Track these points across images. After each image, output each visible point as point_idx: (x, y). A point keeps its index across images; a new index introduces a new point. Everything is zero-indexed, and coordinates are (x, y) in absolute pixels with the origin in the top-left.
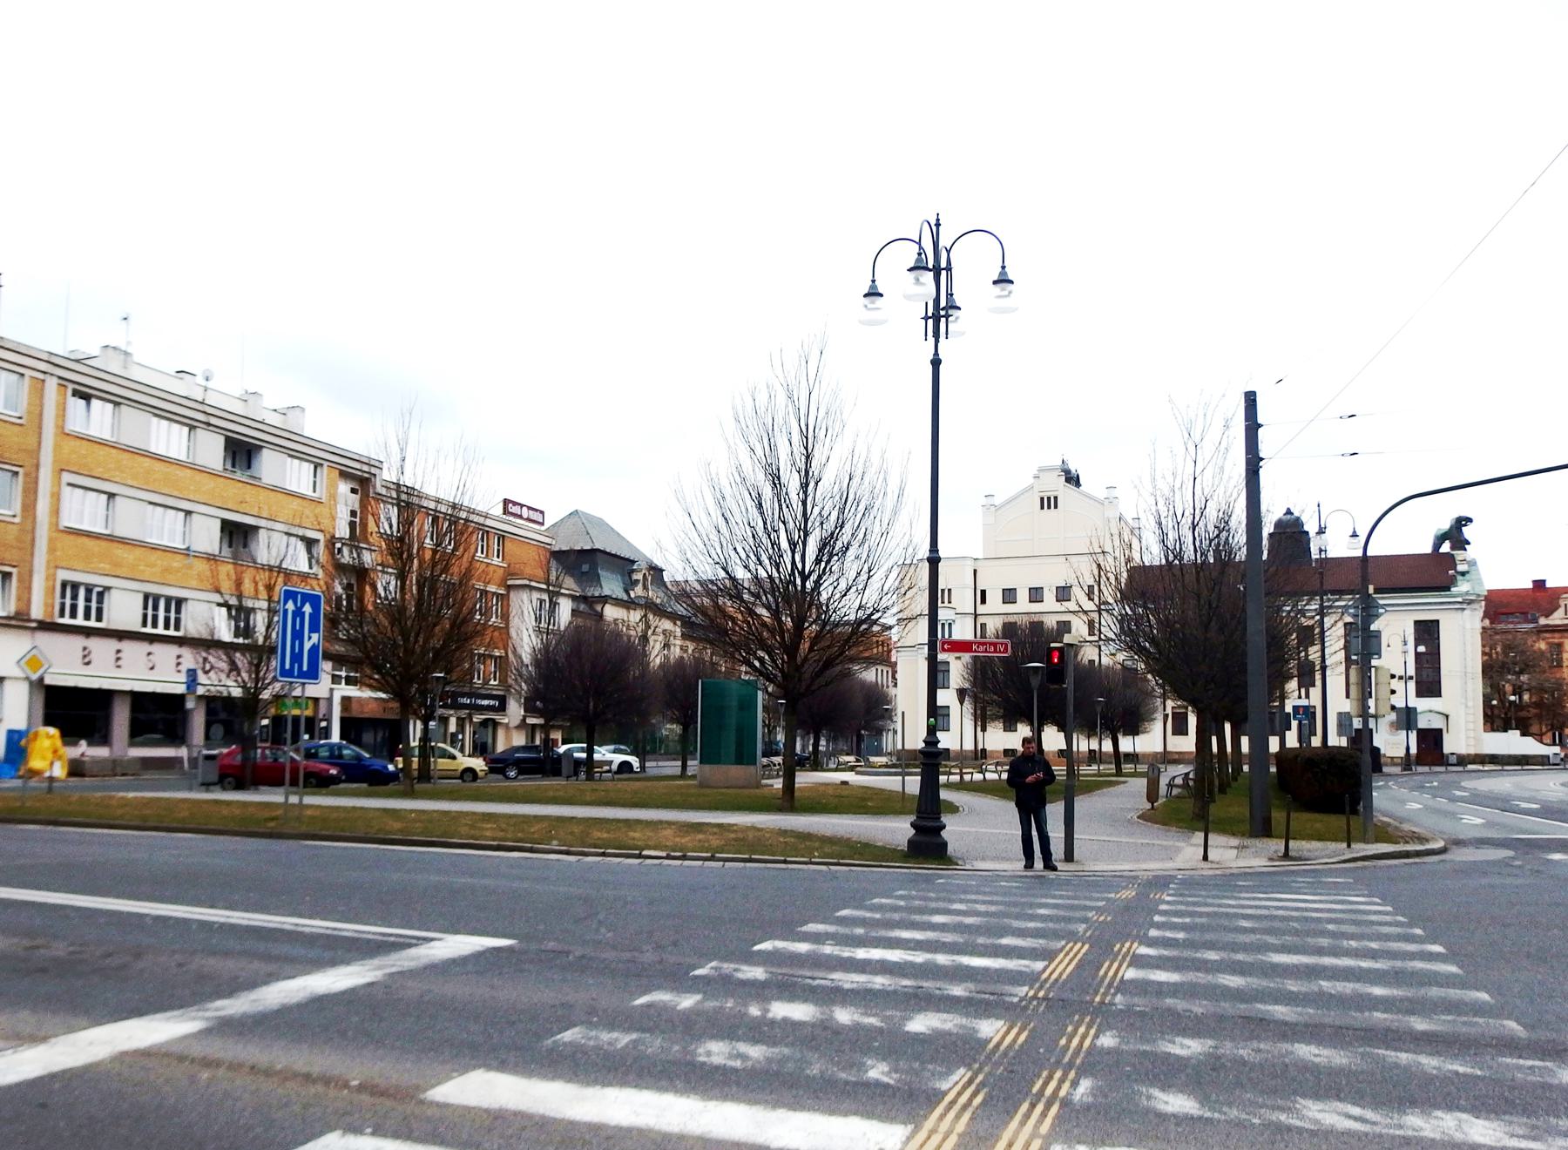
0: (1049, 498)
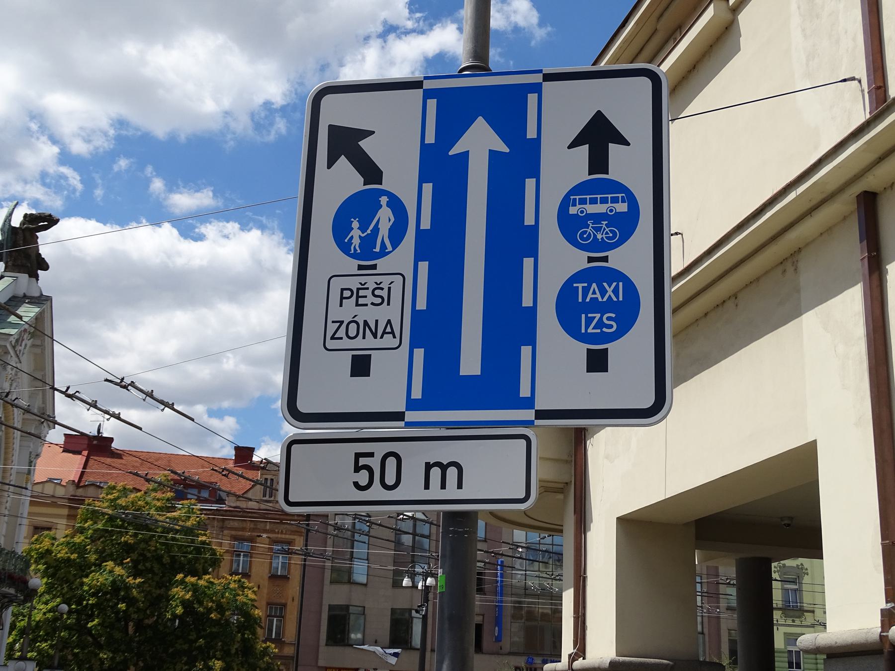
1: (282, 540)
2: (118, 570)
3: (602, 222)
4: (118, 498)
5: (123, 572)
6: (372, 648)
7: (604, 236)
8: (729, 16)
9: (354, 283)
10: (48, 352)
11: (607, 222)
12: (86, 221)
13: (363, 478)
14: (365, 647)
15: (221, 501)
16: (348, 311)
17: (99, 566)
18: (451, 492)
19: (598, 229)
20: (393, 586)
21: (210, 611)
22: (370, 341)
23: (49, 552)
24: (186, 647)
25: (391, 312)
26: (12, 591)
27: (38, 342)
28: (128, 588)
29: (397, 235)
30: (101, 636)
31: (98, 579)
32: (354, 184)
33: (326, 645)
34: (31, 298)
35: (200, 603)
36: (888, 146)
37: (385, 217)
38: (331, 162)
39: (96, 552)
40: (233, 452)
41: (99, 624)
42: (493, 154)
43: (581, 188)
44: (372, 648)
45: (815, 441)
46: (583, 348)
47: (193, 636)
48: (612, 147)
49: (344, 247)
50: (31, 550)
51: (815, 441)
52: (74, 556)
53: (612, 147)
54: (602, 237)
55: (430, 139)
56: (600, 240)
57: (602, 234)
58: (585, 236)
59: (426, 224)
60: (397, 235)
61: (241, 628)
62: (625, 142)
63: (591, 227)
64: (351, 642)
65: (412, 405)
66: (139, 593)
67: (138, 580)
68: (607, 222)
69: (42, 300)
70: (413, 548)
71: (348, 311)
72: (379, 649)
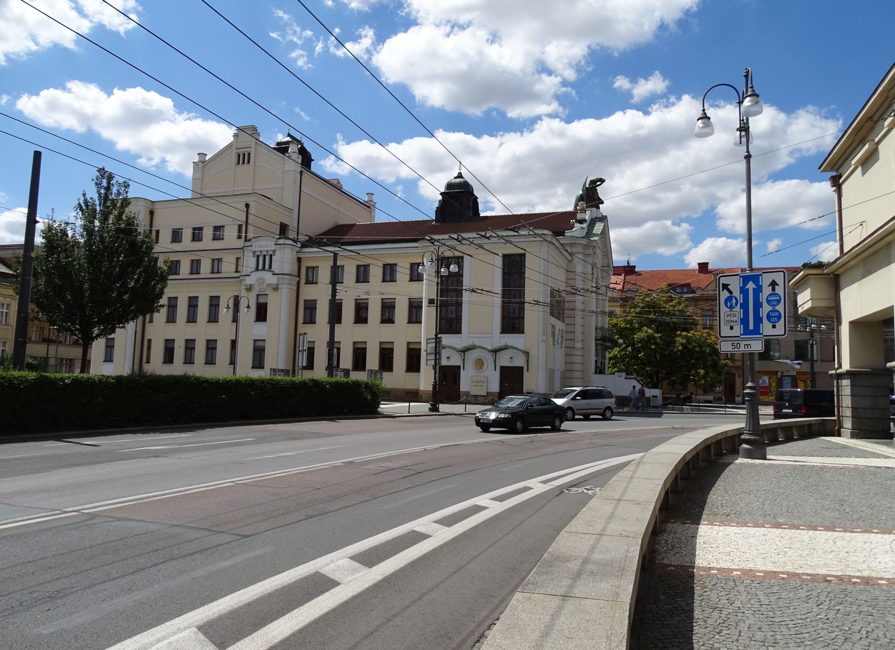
0: (244, 155)
2: (650, 331)
4: (645, 298)
5: (652, 331)
6: (785, 361)
8: (876, 146)
9: (729, 313)
10: (607, 236)
13: (734, 347)
14: (781, 360)
15: (694, 292)
16: (728, 318)
17: (640, 329)
18: (749, 349)
21: (695, 347)
22: (733, 324)
23: (616, 324)
24: (685, 364)
25: (736, 318)
26: (610, 344)
27: (603, 236)
28: (655, 338)
29: (736, 304)
30: (645, 360)
31: (638, 336)
32: (728, 294)
33: (759, 360)
34: (599, 218)
35: (690, 344)
36: (892, 229)
37: (734, 301)
38: (723, 291)
39: (638, 323)
40: (698, 266)
41: (644, 355)
42: (754, 288)
43: (770, 295)
44: (785, 361)
45: (893, 306)
46: (771, 324)
47: (688, 359)
48: (776, 287)
49: (727, 307)
51: (893, 306)
52: (628, 326)
55: (741, 285)
59: (742, 302)
60: (736, 304)
61: (710, 354)
64: (772, 358)
65: (741, 335)
66: (660, 341)
67: (659, 335)
69: (603, 219)
71: (728, 318)
72: (789, 361)
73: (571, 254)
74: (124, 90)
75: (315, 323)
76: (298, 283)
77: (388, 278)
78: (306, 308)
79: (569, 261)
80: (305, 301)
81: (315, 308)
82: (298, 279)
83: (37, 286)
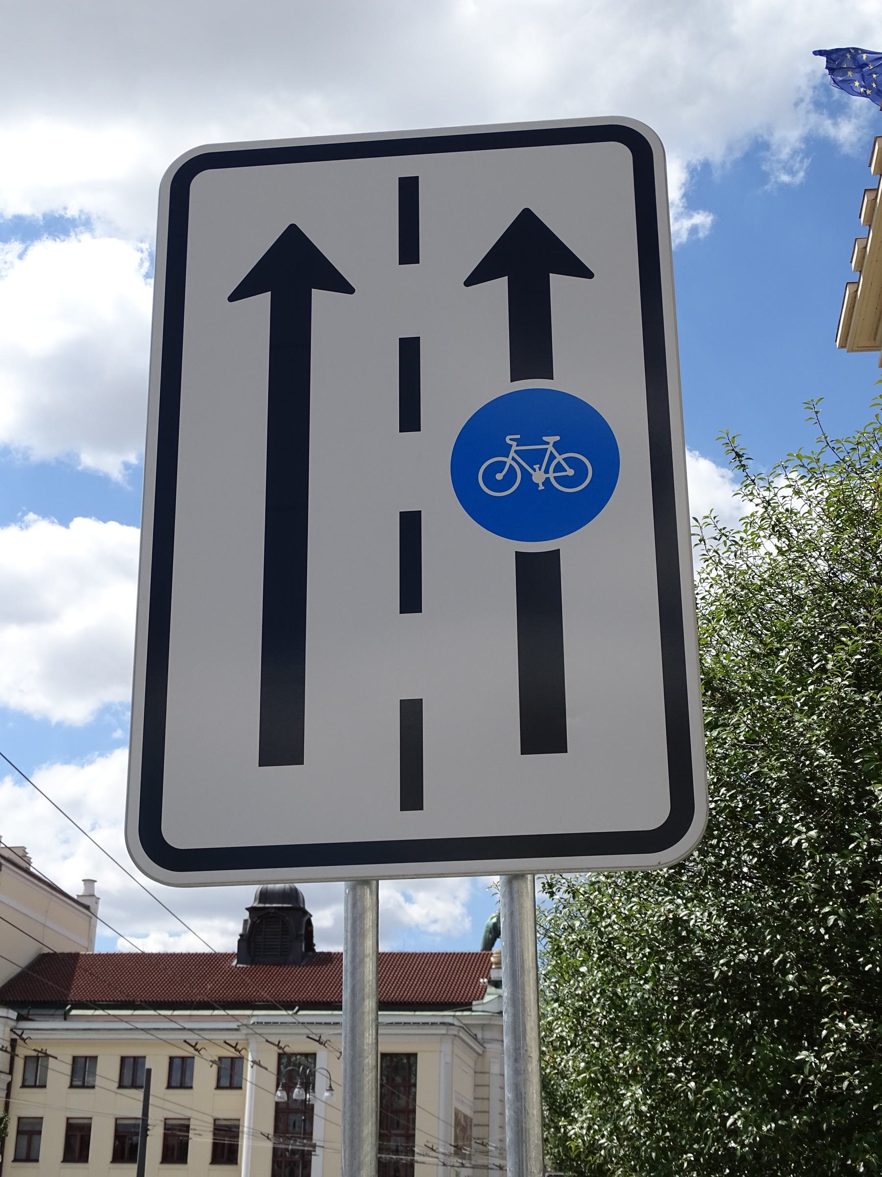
1: (349, 937)
3: (544, 438)
7: (551, 475)
11: (558, 438)
12: (147, 276)
19: (534, 458)
20: (187, 1128)
48: (319, 297)
50: (731, 714)
53: (319, 297)
54: (548, 479)
56: (541, 487)
57: (546, 472)
58: (499, 476)
62: (344, 286)
63: (515, 451)
68: (558, 438)
70: (641, 977)
73: (481, 1044)
74: (105, 522)
75: (37, 1161)
76: (9, 1085)
77: (225, 1082)
78: (19, 1133)
79: (479, 1054)
80: (19, 1118)
81: (39, 1133)
82: (8, 1078)
83: (744, 1140)
